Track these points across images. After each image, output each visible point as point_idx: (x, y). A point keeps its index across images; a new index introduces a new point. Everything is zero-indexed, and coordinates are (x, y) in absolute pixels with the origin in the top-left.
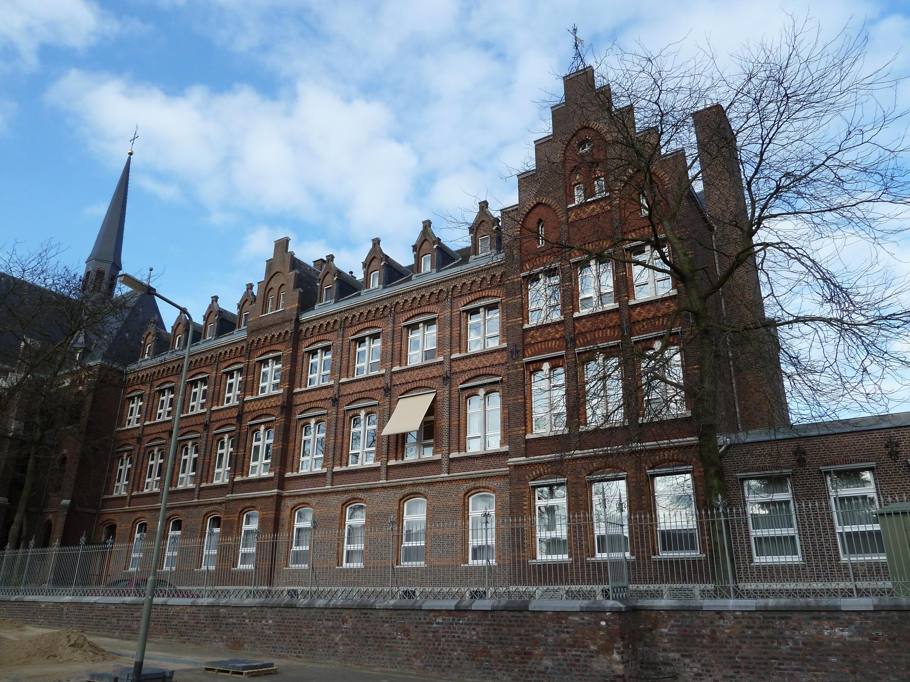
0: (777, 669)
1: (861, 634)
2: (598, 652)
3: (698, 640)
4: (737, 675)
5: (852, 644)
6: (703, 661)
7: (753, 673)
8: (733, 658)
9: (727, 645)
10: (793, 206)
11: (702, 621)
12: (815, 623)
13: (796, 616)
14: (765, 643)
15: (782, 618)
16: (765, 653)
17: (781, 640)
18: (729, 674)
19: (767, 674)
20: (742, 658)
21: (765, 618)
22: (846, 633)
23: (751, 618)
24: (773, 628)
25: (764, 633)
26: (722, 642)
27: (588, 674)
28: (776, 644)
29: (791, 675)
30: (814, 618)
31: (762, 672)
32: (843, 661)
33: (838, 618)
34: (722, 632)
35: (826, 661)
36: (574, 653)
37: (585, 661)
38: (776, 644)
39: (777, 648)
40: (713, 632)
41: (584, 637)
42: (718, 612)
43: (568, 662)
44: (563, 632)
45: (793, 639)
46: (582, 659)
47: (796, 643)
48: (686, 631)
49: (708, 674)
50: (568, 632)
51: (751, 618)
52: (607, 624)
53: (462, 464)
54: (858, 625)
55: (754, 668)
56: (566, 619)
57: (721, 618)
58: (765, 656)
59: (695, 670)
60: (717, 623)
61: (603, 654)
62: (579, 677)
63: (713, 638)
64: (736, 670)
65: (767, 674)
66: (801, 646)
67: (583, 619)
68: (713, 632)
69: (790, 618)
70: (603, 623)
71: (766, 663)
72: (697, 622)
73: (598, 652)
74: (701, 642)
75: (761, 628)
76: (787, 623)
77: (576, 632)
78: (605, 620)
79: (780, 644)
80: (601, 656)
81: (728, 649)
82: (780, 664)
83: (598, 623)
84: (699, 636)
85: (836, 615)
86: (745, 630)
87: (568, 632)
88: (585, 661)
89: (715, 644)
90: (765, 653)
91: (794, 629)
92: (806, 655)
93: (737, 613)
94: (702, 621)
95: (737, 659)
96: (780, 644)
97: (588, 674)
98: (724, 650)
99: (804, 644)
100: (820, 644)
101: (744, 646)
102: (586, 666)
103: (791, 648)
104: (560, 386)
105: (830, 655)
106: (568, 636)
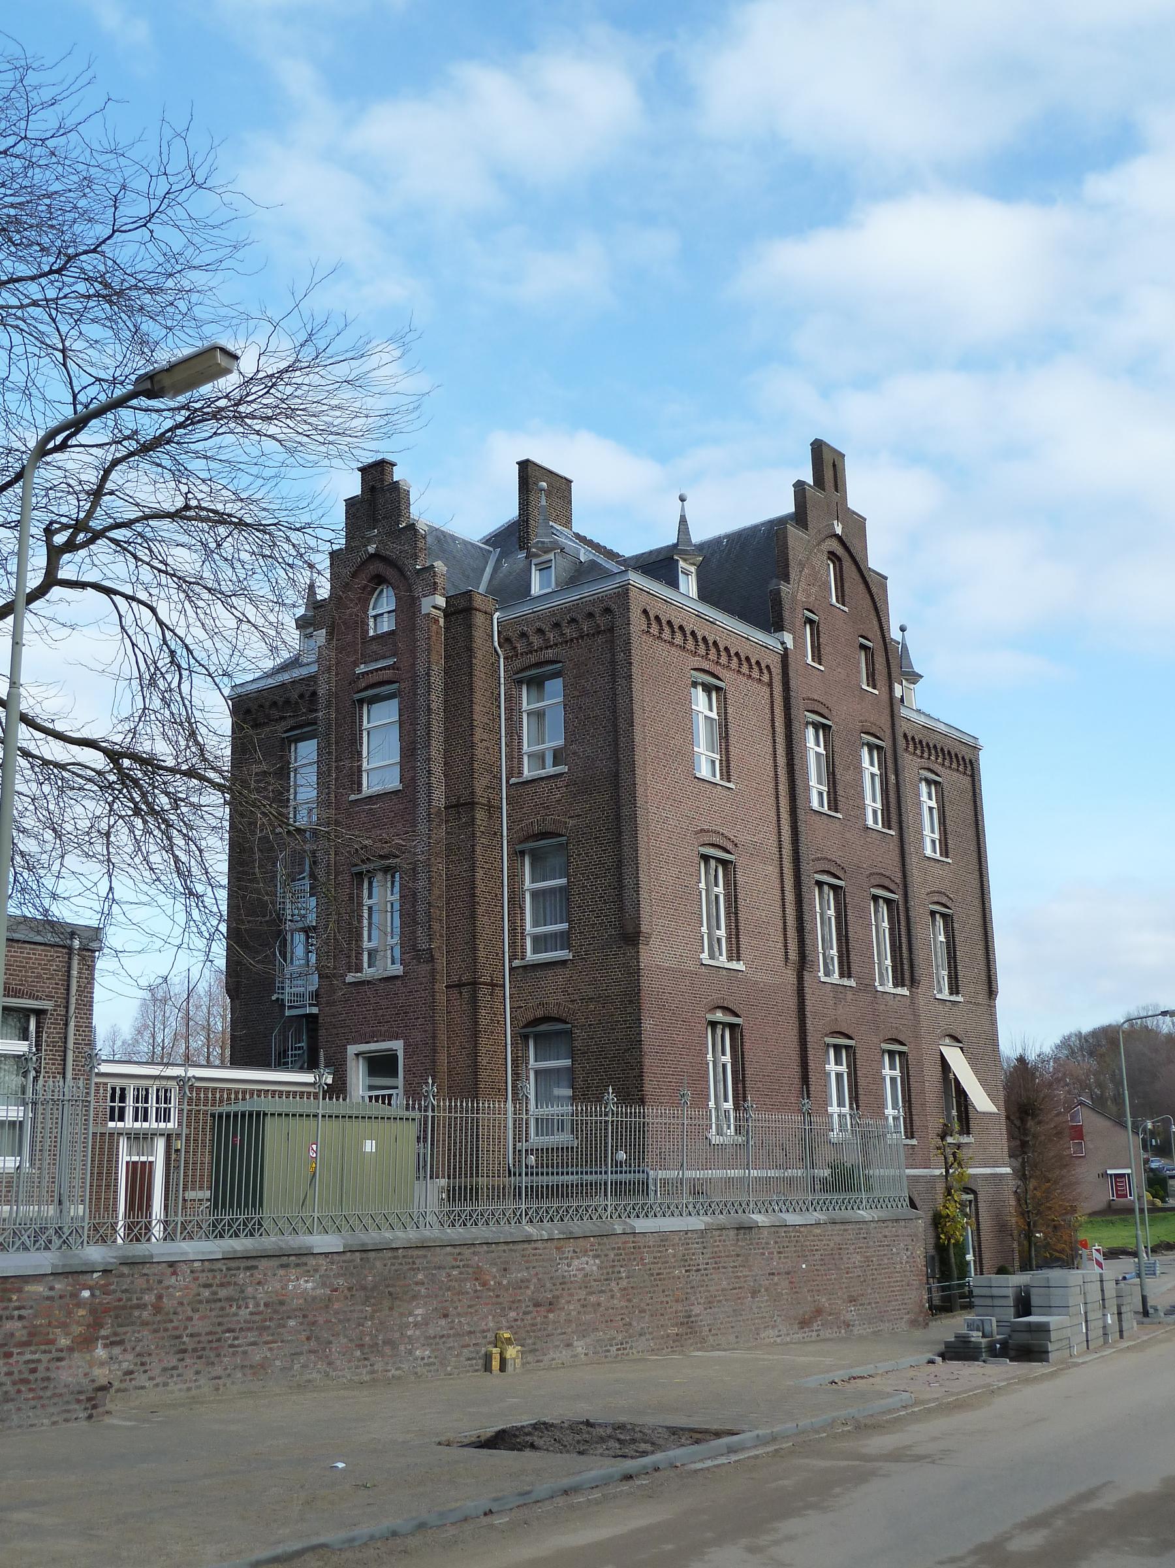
0: (231, 1346)
1: (324, 1285)
2: (71, 1349)
3: (136, 1313)
4: (181, 1364)
5: (314, 1298)
6: (138, 1349)
7: (200, 1357)
8: (180, 1337)
9: (174, 1318)
10: (112, 540)
11: (148, 1281)
12: (281, 1272)
13: (263, 1264)
14: (222, 1309)
15: (248, 1268)
16: (220, 1324)
17: (241, 1302)
18: (172, 1364)
19: (218, 1355)
20: (192, 1335)
21: (229, 1269)
22: (310, 1285)
23: (212, 1270)
24: (235, 1284)
25: (223, 1293)
26: (167, 1314)
27: (49, 1393)
28: (234, 1309)
29: (245, 1353)
30: (282, 1266)
31: (212, 1354)
32: (302, 1323)
33: (306, 1264)
34: (171, 1296)
35: (284, 1326)
36: (28, 1357)
37: (48, 1369)
38: (234, 1309)
39: (236, 1315)
40: (160, 1297)
41: (50, 1324)
42: (171, 1264)
43: (16, 1377)
44: (12, 1318)
45: (254, 1298)
46: (41, 1367)
47: (258, 1305)
48: (120, 1300)
49: (143, 1368)
50: (20, 1318)
51: (212, 1270)
52: (92, 1295)
53: (806, 917)
54: (323, 1272)
55: (204, 1349)
56: (20, 1290)
57: (174, 1273)
58: (219, 1329)
59: (125, 1365)
60: (166, 1283)
61: (80, 1351)
62: (32, 1403)
63: (158, 1309)
64: (181, 1356)
65: (218, 1355)
66: (262, 1308)
67: (52, 1289)
68: (160, 1297)
69: (256, 1267)
70: (86, 1294)
71: (219, 1340)
72: (140, 1283)
73: (71, 1349)
74: (140, 1317)
75: (222, 1285)
76: (252, 1275)
77: (35, 1316)
78: (91, 1288)
79: (239, 1307)
80: (76, 1355)
81: (175, 1324)
82: (235, 1338)
83: (75, 1295)
84: (138, 1307)
85: (304, 1259)
86: (201, 1289)
87: (20, 1318)
88: (48, 1369)
89: (158, 1318)
90: (220, 1324)
91: (259, 1283)
92: (265, 1321)
93: (196, 1264)
94: (148, 1281)
95: (185, 1339)
96: (239, 1307)
97: (49, 1393)
98: (170, 1326)
99: (266, 1305)
100: (282, 1303)
101: (196, 1316)
102: (48, 1379)
103: (251, 1314)
104: (310, 764)
105: (289, 1318)
106: (19, 1324)
